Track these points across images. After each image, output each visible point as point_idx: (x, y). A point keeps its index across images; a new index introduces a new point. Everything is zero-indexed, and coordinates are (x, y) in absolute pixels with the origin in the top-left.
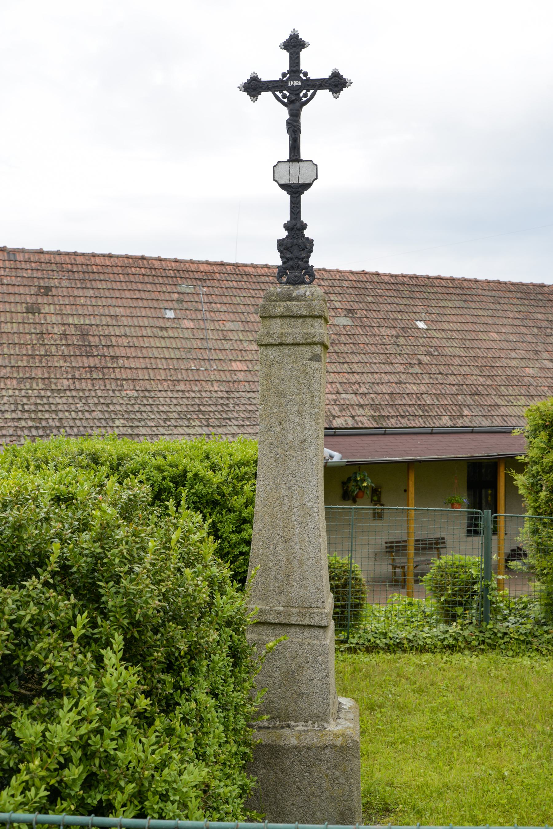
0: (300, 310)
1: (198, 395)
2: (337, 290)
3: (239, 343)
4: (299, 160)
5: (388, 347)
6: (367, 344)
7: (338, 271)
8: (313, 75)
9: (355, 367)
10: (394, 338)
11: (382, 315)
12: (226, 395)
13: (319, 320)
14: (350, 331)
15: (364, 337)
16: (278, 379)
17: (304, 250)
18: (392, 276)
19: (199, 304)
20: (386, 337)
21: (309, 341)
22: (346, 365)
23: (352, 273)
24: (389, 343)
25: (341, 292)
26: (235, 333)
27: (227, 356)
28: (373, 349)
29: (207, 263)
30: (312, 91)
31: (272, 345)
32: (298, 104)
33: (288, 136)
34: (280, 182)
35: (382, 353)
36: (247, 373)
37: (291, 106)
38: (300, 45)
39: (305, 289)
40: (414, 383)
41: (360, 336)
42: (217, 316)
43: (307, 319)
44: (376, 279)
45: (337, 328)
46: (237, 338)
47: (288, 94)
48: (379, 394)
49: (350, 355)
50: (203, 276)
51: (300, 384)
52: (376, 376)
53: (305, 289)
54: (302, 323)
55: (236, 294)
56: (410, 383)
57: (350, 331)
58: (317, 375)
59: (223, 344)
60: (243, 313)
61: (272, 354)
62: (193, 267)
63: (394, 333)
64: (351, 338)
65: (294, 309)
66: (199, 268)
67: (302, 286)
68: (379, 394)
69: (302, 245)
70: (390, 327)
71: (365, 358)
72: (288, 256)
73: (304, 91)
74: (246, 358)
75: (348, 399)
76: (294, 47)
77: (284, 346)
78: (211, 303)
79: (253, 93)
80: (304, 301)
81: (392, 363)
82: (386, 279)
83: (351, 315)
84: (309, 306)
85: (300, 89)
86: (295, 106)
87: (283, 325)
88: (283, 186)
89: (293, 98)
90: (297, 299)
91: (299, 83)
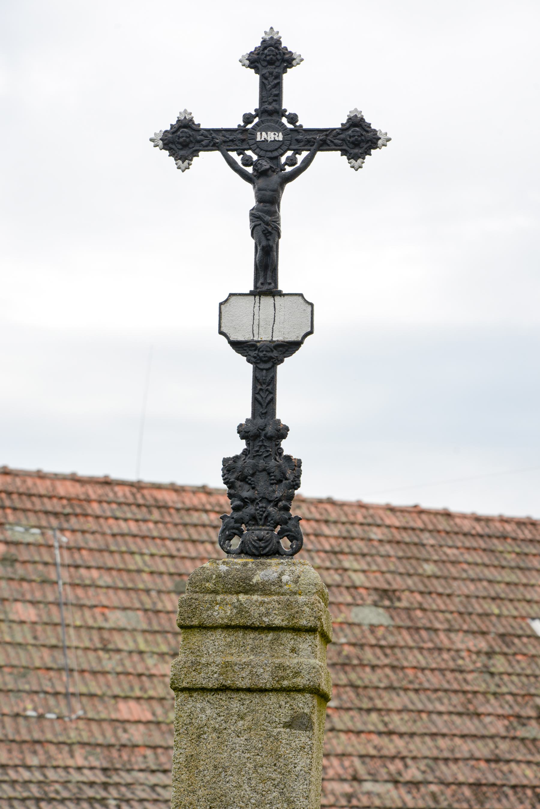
0: (267, 614)
1: (37, 776)
2: (358, 546)
3: (136, 657)
4: (274, 293)
5: (470, 677)
6: (423, 669)
7: (361, 506)
8: (307, 122)
9: (397, 722)
10: (484, 658)
11: (456, 604)
12: (101, 778)
13: (309, 637)
14: (385, 638)
15: (416, 652)
16: (215, 767)
17: (280, 481)
18: (478, 519)
19: (51, 569)
20: (464, 654)
21: (285, 683)
22: (374, 716)
23: (392, 509)
24: (471, 667)
25: (365, 550)
26: (128, 636)
27: (109, 686)
28: (435, 680)
29: (75, 479)
30: (305, 154)
31: (203, 690)
32: (275, 178)
33: (252, 242)
34: (233, 338)
35: (456, 692)
36: (152, 727)
37: (261, 182)
38: (284, 61)
39: (280, 569)
40: (529, 763)
41: (407, 651)
42: (89, 597)
43: (282, 634)
44: (443, 524)
45: (357, 630)
46: (131, 646)
47: (255, 158)
48: (448, 785)
49: (384, 694)
50: (64, 507)
51: (263, 781)
52: (442, 743)
53: (280, 569)
54: (272, 642)
55: (134, 548)
56: (518, 762)
57: (385, 638)
58: (302, 762)
59: (99, 659)
60: (147, 591)
61: (203, 710)
62: (42, 487)
63: (483, 645)
64: (386, 655)
65: (255, 612)
66: (54, 488)
67: (274, 561)
68: (448, 785)
69: (277, 473)
70: (473, 633)
71: (418, 701)
72: (246, 493)
73: (289, 153)
74: (151, 693)
75: (379, 795)
76: (271, 63)
77: (229, 694)
78: (77, 567)
79: (182, 153)
80: (278, 594)
81: (478, 715)
82: (467, 525)
83: (387, 603)
84: (288, 605)
85: (281, 147)
86: (269, 181)
87: (229, 645)
88: (238, 346)
89: (266, 165)
90: (263, 589)
91: (280, 137)
